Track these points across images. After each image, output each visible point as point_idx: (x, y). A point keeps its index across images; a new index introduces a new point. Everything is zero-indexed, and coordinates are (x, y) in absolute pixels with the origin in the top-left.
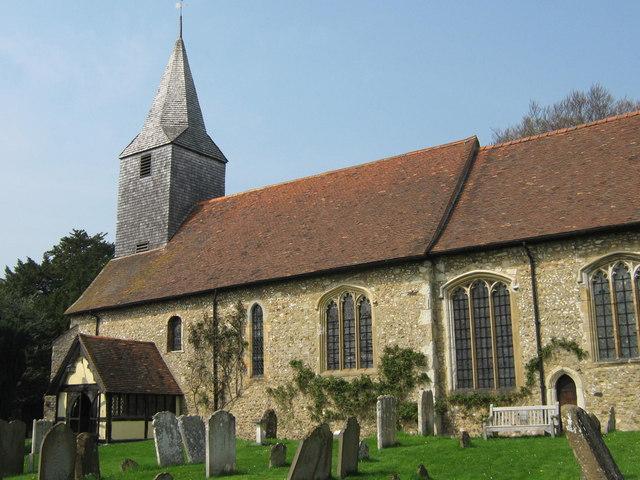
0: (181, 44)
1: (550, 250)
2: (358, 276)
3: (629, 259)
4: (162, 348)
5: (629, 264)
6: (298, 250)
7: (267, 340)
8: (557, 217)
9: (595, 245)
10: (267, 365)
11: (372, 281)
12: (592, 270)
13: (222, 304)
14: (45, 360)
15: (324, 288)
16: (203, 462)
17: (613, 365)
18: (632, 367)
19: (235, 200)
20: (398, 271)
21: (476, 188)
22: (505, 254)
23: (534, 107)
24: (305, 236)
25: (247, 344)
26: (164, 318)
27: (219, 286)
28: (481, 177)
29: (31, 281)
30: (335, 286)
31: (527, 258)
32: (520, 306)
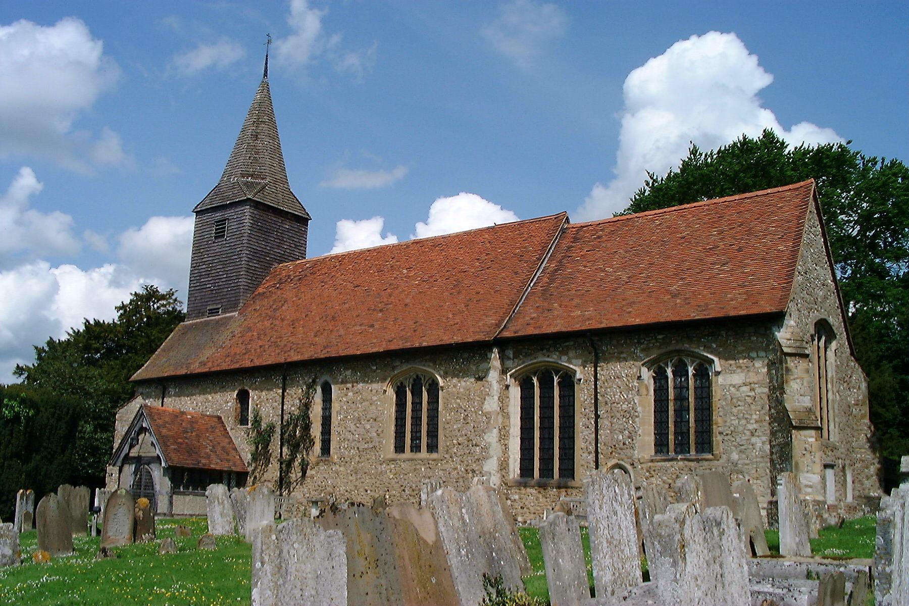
0: (267, 56)
1: (614, 342)
2: (427, 357)
3: (688, 355)
4: (230, 423)
5: (687, 361)
6: (372, 326)
7: (335, 419)
8: (625, 308)
9: (657, 340)
10: (333, 445)
11: (441, 364)
12: (652, 365)
13: (291, 379)
14: (108, 425)
15: (394, 368)
16: (196, 324)
17: (665, 460)
18: (681, 463)
19: (316, 263)
20: (466, 355)
21: (556, 271)
22: (572, 343)
23: (694, 152)
24: (381, 311)
25: (846, 594)
26: (761, 511)
27: (289, 360)
28: (563, 257)
29: (97, 338)
30: (405, 367)
31: (591, 348)
32: (583, 396)
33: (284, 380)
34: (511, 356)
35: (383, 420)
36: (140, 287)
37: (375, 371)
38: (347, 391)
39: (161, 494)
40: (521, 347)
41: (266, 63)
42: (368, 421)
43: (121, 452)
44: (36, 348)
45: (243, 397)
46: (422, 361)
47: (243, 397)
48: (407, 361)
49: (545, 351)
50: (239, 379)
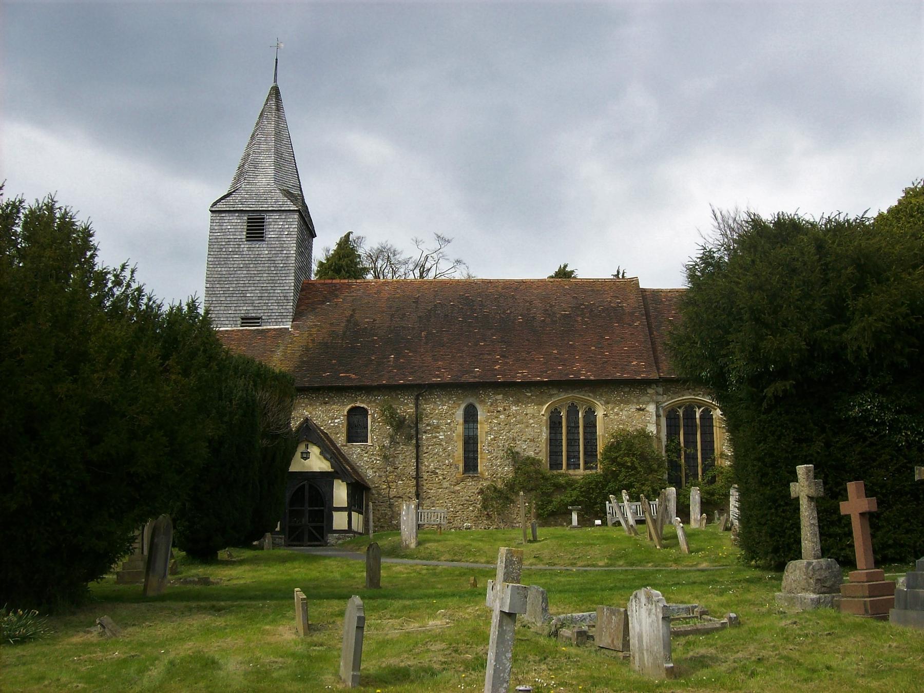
20: (627, 390)
30: (563, 396)
33: (417, 399)
34: (661, 393)
35: (541, 441)
36: (361, 235)
37: (529, 398)
38: (498, 414)
39: (604, 530)
40: (669, 386)
41: (276, 75)
42: (525, 441)
43: (297, 546)
44: (57, 201)
45: (470, 416)
46: (582, 391)
47: (470, 416)
48: (566, 391)
49: (690, 390)
50: (348, 396)
